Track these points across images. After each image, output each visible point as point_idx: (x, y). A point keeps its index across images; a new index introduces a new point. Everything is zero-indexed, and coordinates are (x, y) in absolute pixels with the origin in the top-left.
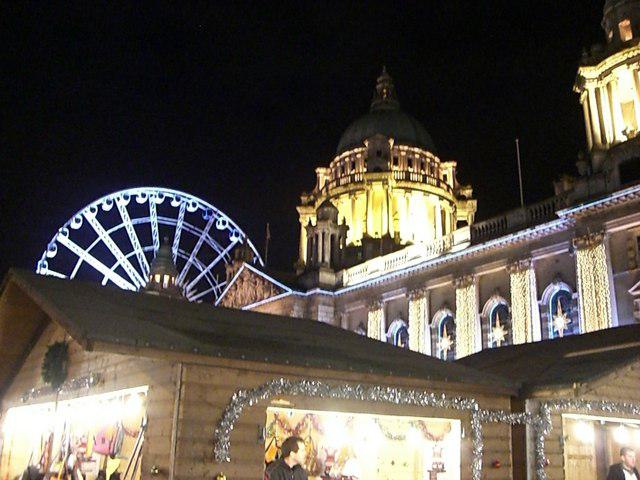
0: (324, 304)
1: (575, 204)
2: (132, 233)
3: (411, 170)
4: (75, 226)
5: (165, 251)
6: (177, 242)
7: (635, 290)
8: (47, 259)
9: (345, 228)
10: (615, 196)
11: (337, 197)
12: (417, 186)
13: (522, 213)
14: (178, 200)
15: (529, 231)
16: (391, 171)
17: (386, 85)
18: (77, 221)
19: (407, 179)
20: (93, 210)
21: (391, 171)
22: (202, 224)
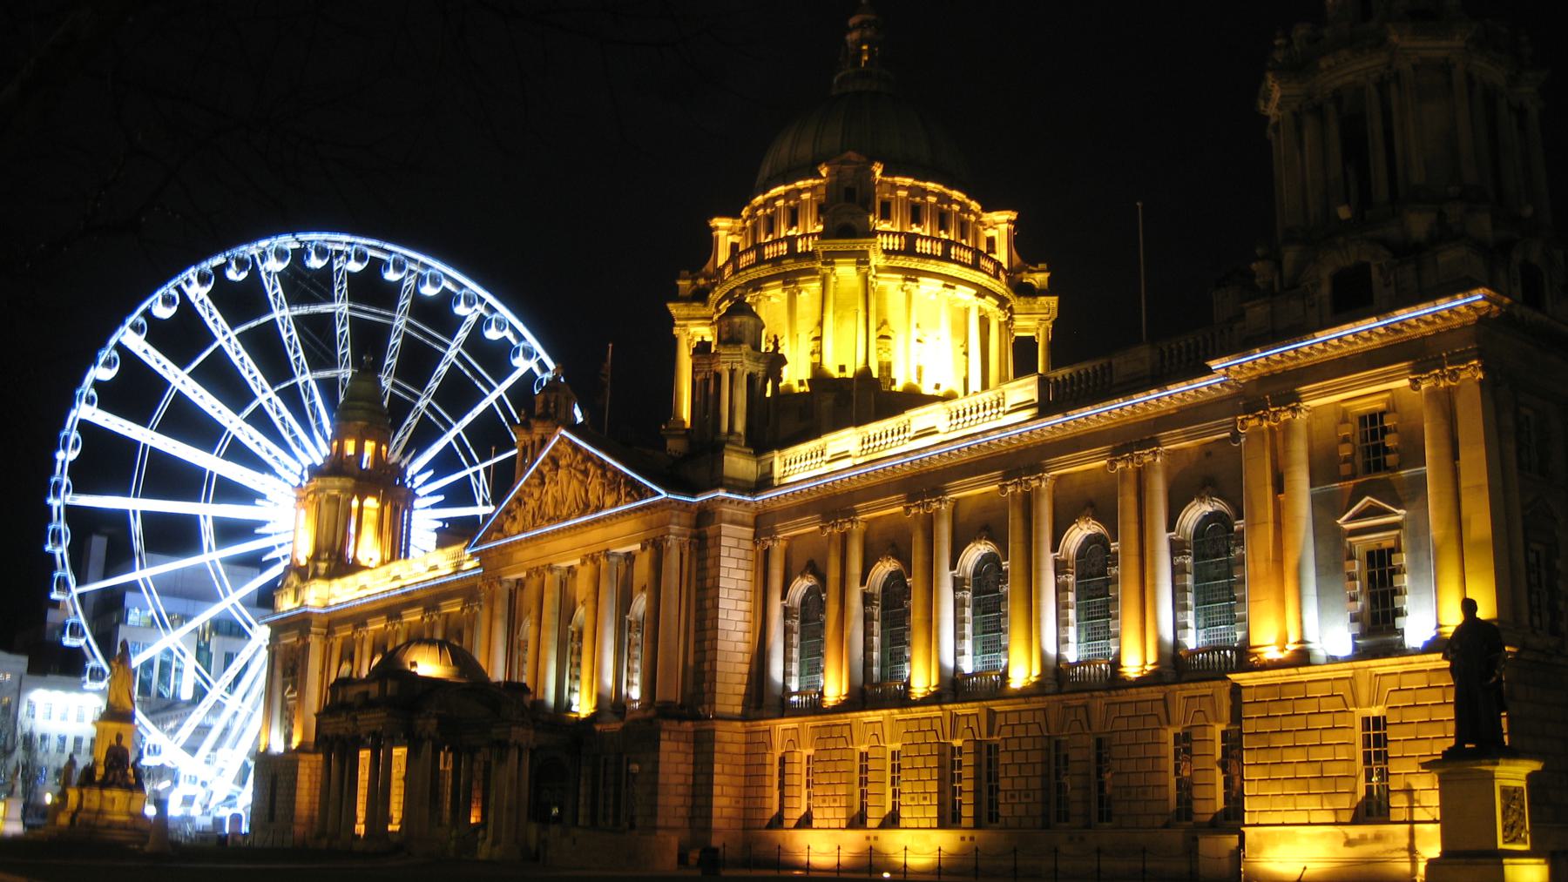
0: (733, 522)
1: (1244, 347)
2: (290, 335)
3: (916, 229)
4: (163, 312)
5: (365, 386)
6: (391, 361)
7: (1350, 520)
8: (97, 384)
9: (776, 361)
10: (1321, 336)
11: (757, 285)
12: (931, 266)
13: (1143, 356)
14: (399, 267)
15: (1154, 394)
16: (874, 234)
17: (868, 33)
18: (168, 301)
19: (909, 251)
20: (203, 280)
21: (874, 234)
22: (450, 325)
